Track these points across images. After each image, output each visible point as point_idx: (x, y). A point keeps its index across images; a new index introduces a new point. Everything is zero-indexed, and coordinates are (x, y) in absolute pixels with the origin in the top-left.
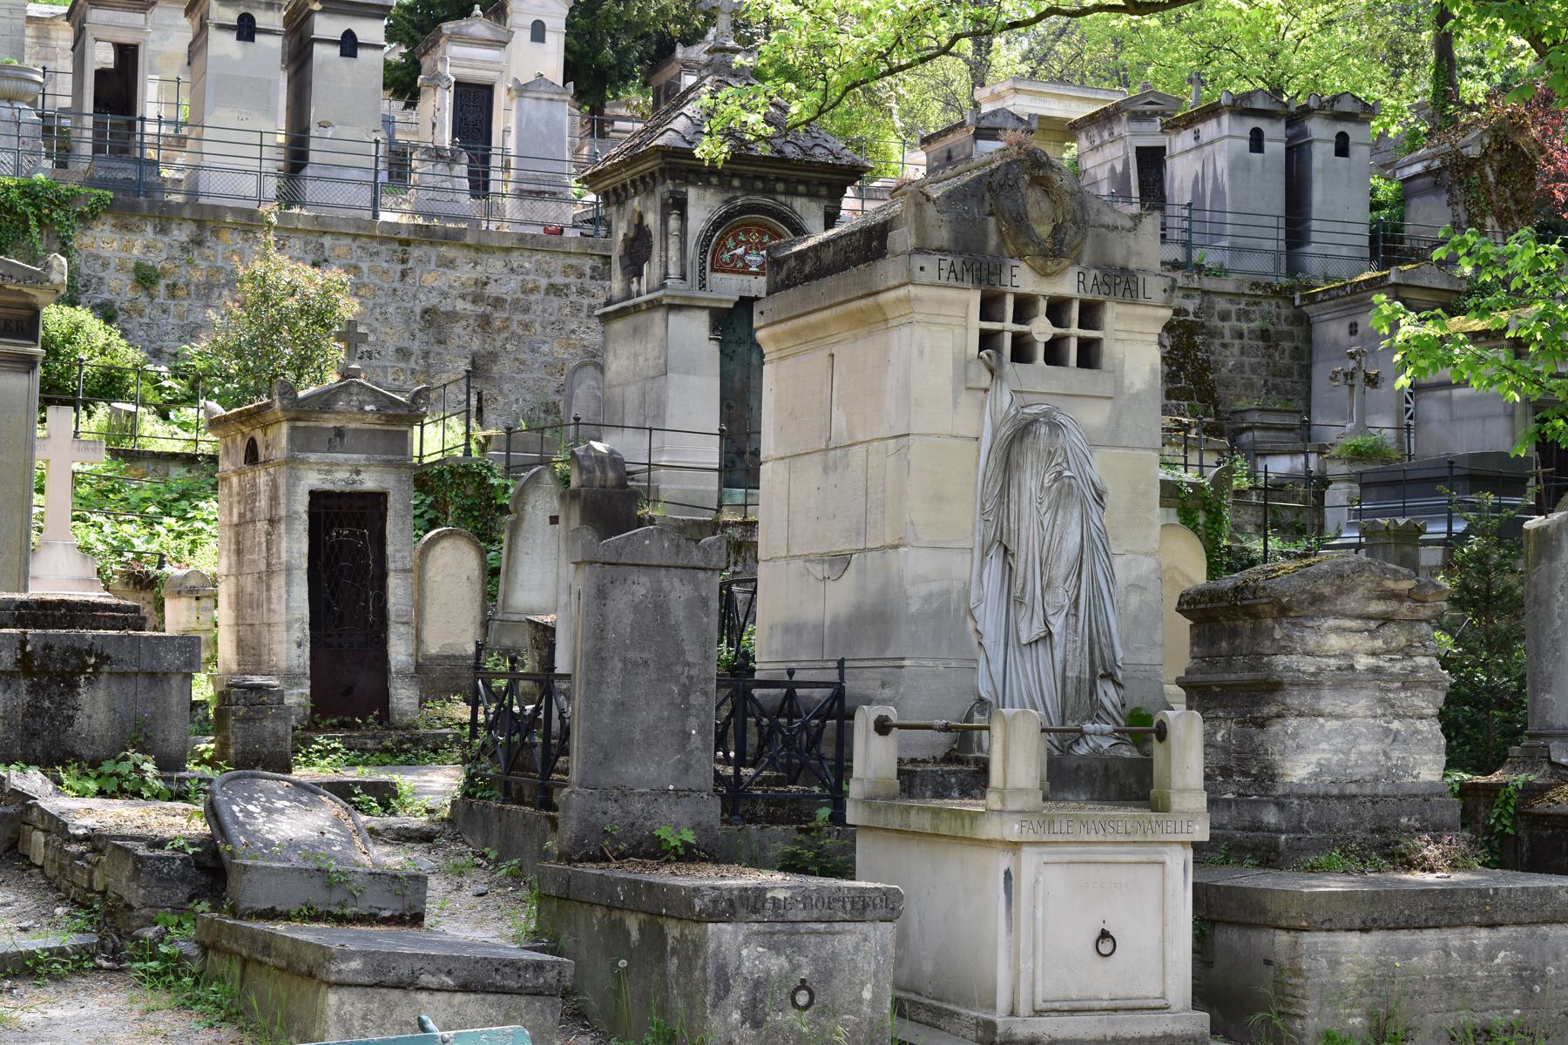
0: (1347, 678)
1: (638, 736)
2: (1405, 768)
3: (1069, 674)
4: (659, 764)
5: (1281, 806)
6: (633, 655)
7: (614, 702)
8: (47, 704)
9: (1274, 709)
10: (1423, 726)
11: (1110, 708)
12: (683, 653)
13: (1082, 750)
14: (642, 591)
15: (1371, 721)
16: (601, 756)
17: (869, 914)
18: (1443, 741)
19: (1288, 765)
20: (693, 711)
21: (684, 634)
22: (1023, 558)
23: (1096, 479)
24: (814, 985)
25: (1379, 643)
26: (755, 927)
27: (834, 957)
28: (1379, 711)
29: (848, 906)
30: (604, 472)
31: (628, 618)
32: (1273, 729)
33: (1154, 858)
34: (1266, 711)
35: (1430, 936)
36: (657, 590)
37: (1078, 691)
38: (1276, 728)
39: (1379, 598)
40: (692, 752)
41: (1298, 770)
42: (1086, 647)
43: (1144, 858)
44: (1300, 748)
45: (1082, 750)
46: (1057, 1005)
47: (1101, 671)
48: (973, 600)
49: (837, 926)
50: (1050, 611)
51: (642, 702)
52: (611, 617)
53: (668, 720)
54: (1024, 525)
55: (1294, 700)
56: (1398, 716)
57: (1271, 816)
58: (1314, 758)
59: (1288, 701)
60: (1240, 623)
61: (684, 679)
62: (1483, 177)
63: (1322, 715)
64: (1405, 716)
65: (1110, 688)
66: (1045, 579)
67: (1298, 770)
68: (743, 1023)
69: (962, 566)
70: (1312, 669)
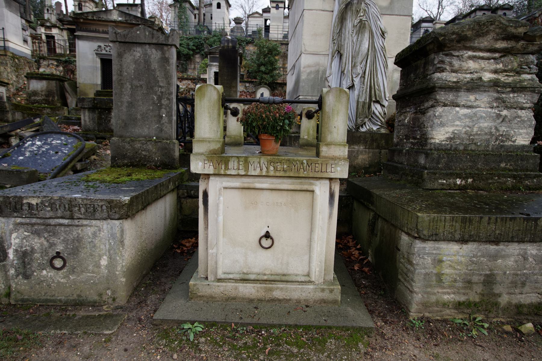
0: (475, 86)
1: (139, 117)
2: (508, 137)
3: (360, 100)
4: (149, 128)
5: (427, 155)
6: (136, 83)
7: (128, 102)
8: (103, 116)
9: (431, 103)
10: (522, 113)
11: (378, 114)
12: (158, 81)
13: (363, 130)
14: (139, 55)
15: (490, 110)
16: (123, 124)
17: (97, 215)
18: (534, 122)
19: (434, 133)
20: (164, 107)
21: (158, 73)
22: (345, 56)
23: (382, 27)
24: (65, 255)
25: (500, 66)
26: (19, 220)
27: (79, 239)
28: (495, 105)
29: (83, 210)
30: (228, 44)
31: (133, 66)
32: (429, 114)
33: (305, 187)
34: (426, 105)
35: (514, 249)
36: (145, 54)
37: (363, 107)
38: (430, 113)
39: (503, 39)
40: (163, 124)
41: (439, 135)
42: (368, 90)
43: (298, 187)
44: (442, 125)
45: (363, 130)
46: (231, 276)
47: (374, 99)
48: (327, 74)
49: (76, 222)
50: (354, 76)
51: (140, 103)
52: (124, 67)
53: (152, 110)
54: (346, 42)
55: (442, 96)
56: (507, 108)
57: (422, 160)
58: (451, 129)
59: (438, 97)
60: (419, 62)
61: (159, 93)
62: (538, 21)
63: (458, 106)
64: (511, 108)
65: (378, 106)
66: (353, 63)
67: (439, 135)
68: (17, 276)
69: (324, 61)
70: (455, 80)
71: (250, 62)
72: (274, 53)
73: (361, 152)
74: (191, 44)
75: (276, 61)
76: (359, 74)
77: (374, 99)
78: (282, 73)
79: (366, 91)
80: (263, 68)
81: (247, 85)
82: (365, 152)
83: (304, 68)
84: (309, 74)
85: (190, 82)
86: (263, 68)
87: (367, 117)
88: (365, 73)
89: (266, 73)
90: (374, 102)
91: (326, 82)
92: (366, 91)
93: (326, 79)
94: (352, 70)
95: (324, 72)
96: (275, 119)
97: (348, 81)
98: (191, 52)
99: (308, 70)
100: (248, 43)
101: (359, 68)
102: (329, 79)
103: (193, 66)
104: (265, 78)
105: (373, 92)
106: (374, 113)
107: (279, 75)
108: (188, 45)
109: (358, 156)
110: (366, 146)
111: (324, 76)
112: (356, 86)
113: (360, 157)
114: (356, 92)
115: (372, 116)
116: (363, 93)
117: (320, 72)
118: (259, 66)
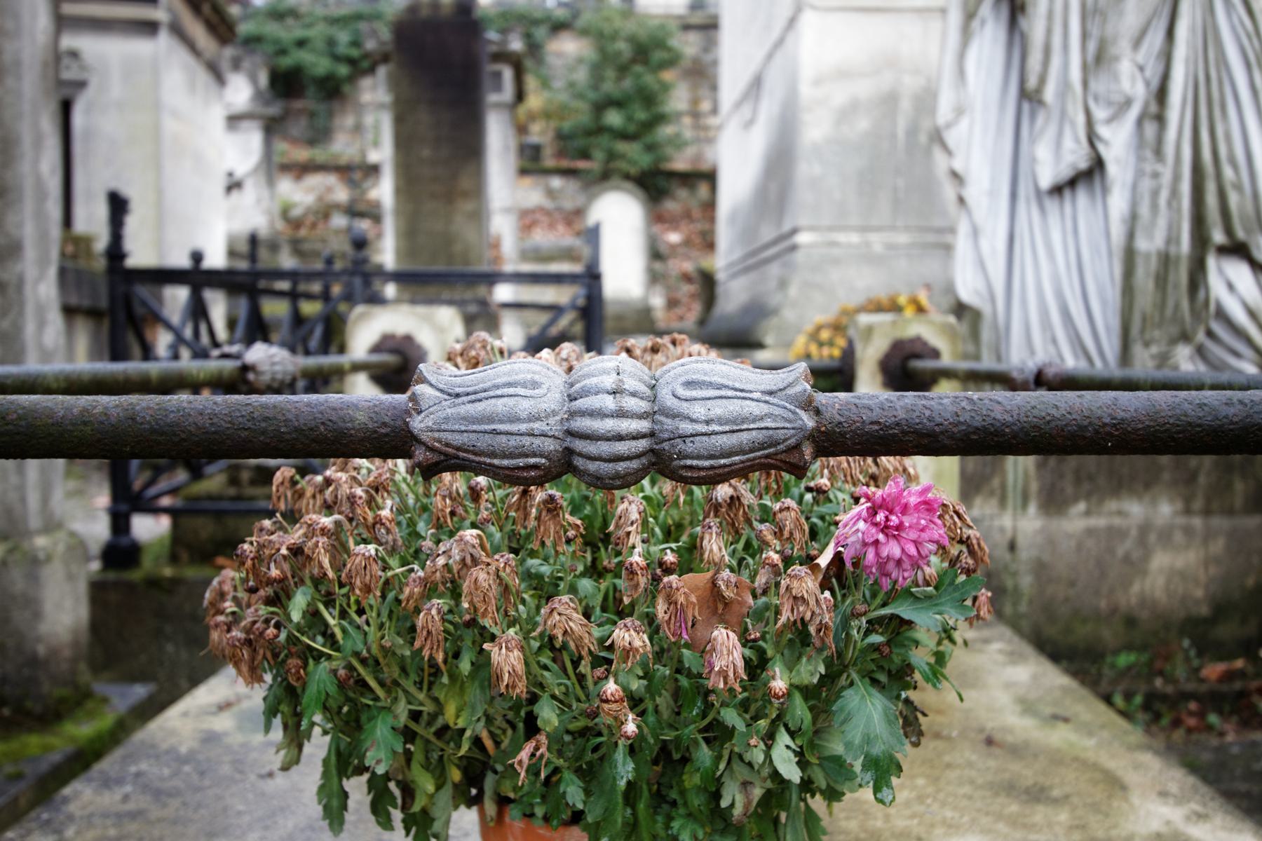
3: (1142, 244)
37: (1162, 280)
42: (1186, 187)
48: (944, 112)
50: (1100, 113)
71: (563, 97)
72: (658, 55)
73: (1166, 537)
74: (343, 37)
75: (666, 87)
76: (1128, 103)
77: (1218, 237)
78: (688, 134)
79: (1175, 192)
80: (614, 118)
81: (556, 182)
82: (1188, 531)
83: (818, 82)
84: (848, 112)
85: (331, 179)
86: (614, 118)
87: (1185, 337)
88: (1161, 94)
89: (624, 136)
90: (1223, 251)
91: (939, 156)
92: (1175, 192)
93: (937, 138)
94: (1085, 84)
95: (926, 100)
96: (677, 682)
97: (1068, 143)
98: (343, 70)
99: (840, 95)
100: (559, 27)
101: (1125, 67)
102: (951, 138)
103: (349, 121)
104: (622, 156)
105: (1211, 200)
106: (1222, 315)
107: (678, 143)
108: (331, 42)
109: (1146, 558)
110: (1188, 501)
111: (926, 125)
112: (1112, 169)
113: (1161, 561)
114: (1118, 202)
115: (1210, 334)
116: (1154, 207)
117: (906, 105)
118: (600, 107)
